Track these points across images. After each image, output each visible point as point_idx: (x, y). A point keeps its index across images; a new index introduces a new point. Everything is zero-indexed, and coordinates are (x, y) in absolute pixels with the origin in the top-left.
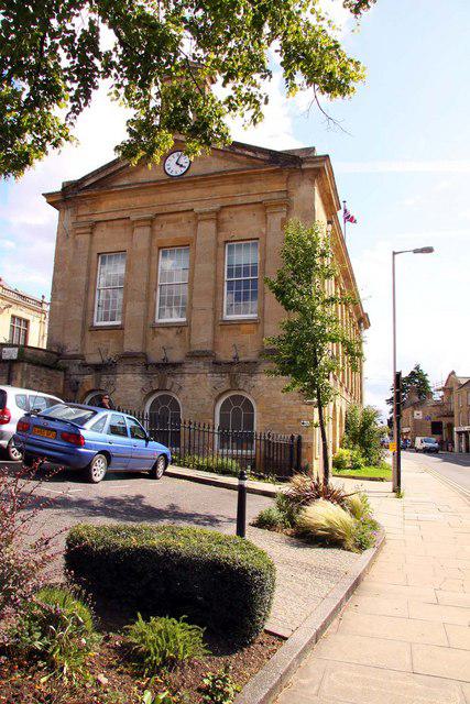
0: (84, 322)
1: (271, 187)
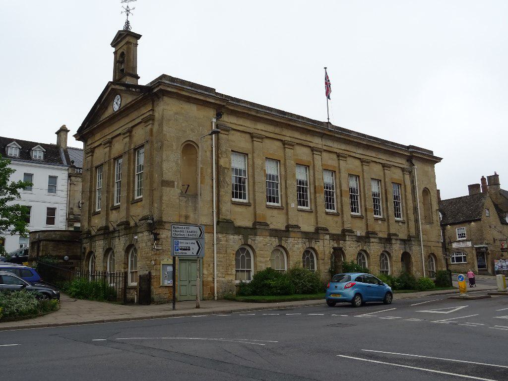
0: (90, 210)
1: (145, 111)
